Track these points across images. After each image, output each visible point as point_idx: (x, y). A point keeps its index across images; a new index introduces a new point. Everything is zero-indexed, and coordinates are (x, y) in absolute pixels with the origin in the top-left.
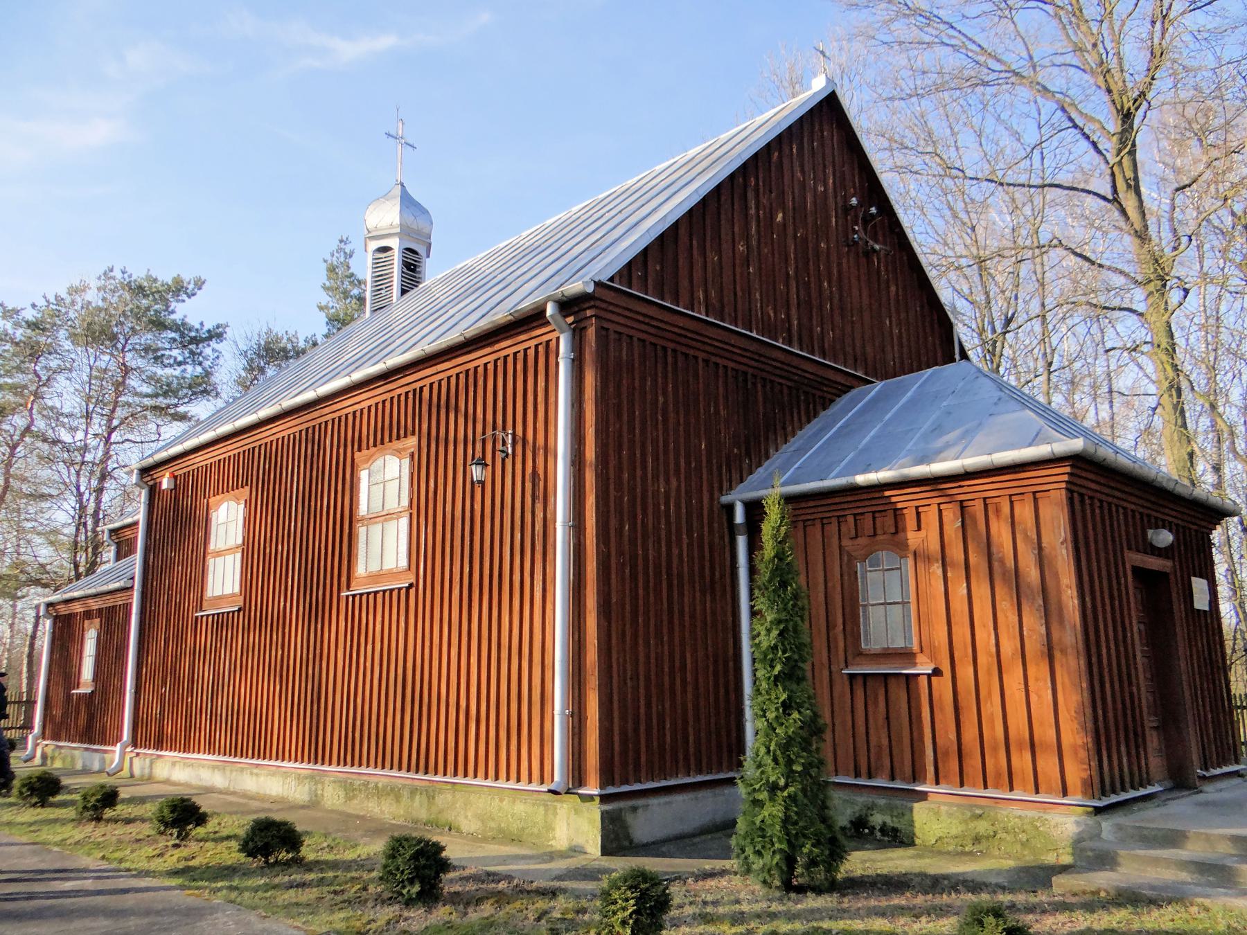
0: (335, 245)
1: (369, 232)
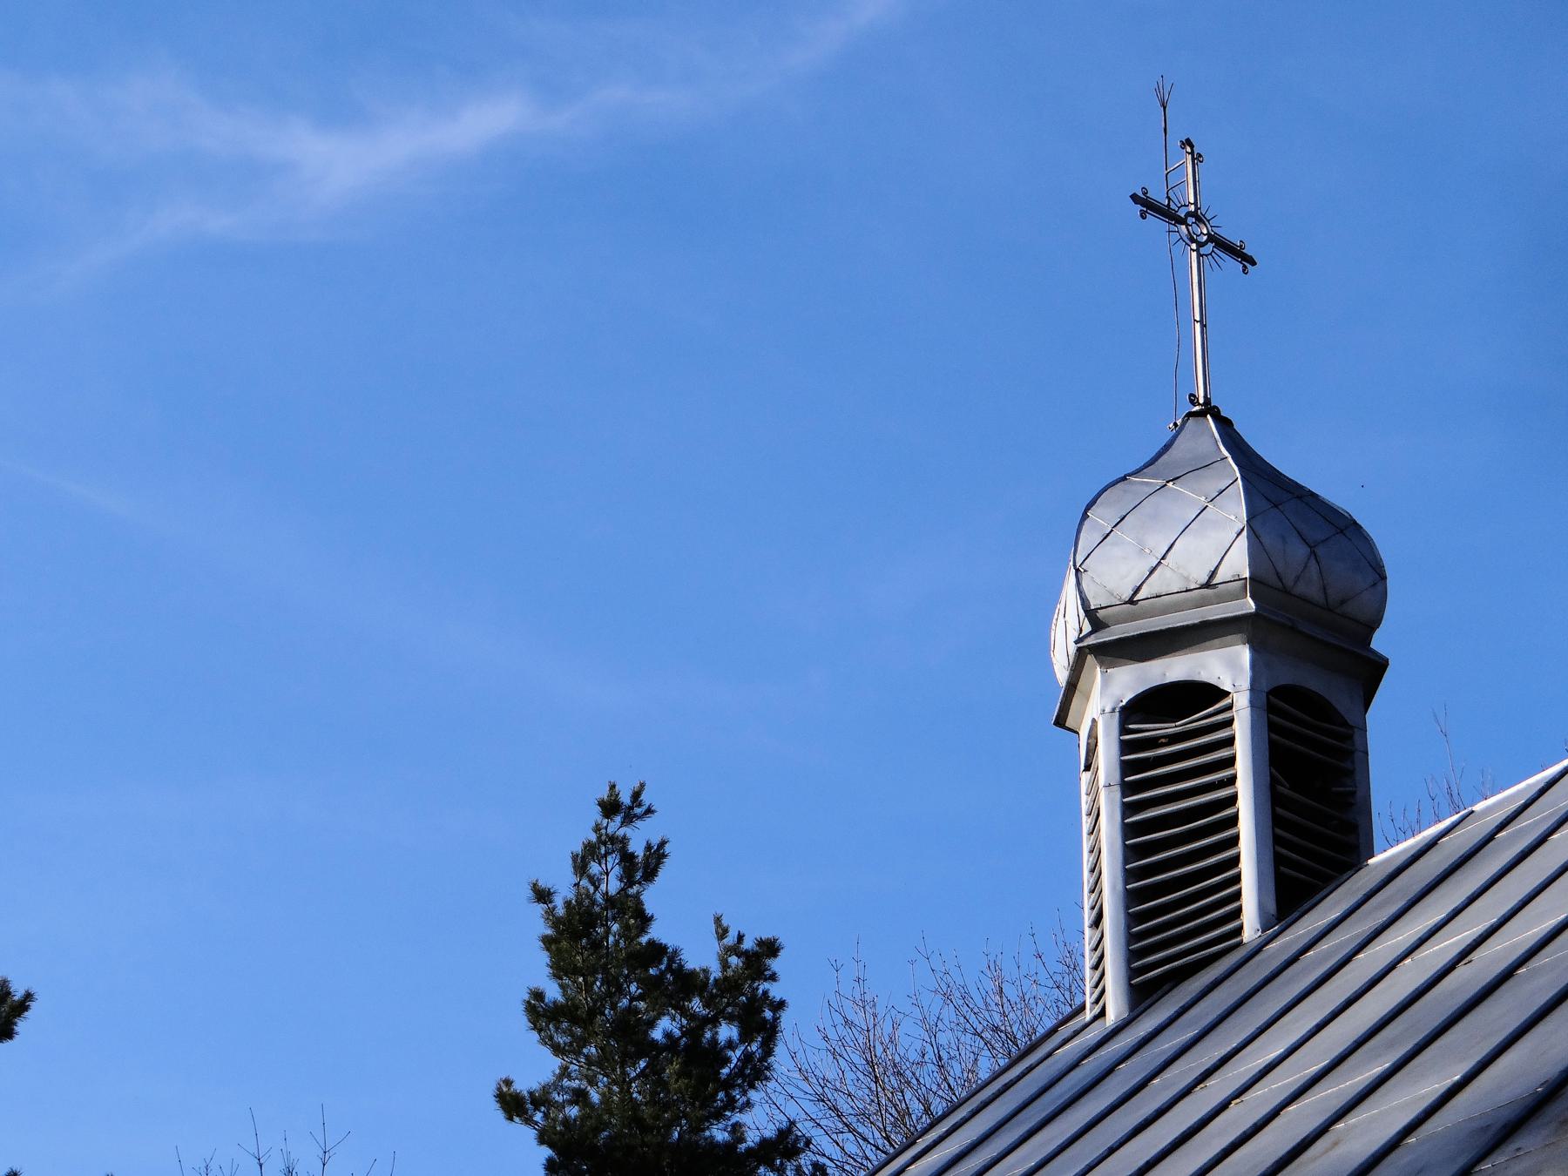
0: (582, 826)
1: (1097, 624)
